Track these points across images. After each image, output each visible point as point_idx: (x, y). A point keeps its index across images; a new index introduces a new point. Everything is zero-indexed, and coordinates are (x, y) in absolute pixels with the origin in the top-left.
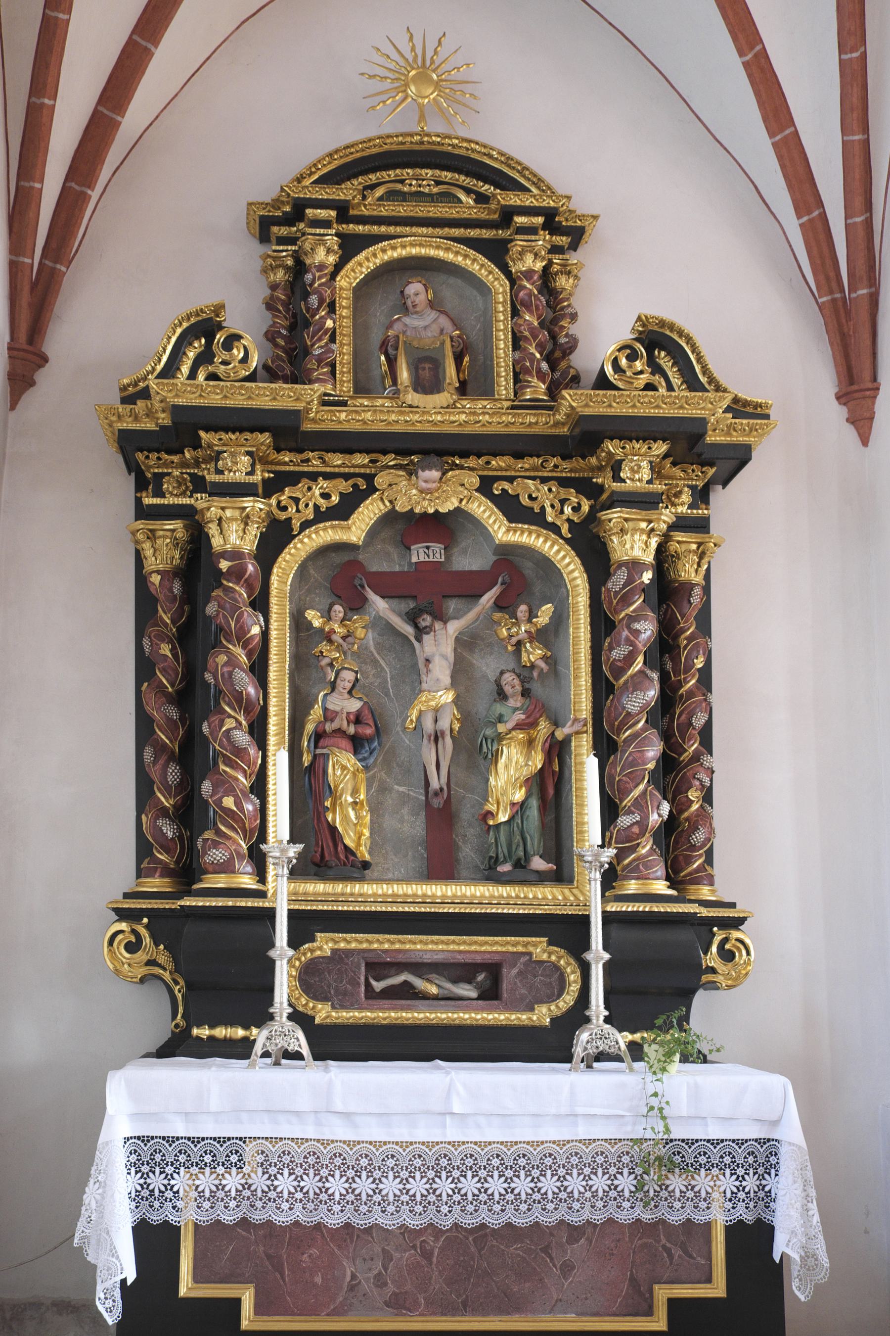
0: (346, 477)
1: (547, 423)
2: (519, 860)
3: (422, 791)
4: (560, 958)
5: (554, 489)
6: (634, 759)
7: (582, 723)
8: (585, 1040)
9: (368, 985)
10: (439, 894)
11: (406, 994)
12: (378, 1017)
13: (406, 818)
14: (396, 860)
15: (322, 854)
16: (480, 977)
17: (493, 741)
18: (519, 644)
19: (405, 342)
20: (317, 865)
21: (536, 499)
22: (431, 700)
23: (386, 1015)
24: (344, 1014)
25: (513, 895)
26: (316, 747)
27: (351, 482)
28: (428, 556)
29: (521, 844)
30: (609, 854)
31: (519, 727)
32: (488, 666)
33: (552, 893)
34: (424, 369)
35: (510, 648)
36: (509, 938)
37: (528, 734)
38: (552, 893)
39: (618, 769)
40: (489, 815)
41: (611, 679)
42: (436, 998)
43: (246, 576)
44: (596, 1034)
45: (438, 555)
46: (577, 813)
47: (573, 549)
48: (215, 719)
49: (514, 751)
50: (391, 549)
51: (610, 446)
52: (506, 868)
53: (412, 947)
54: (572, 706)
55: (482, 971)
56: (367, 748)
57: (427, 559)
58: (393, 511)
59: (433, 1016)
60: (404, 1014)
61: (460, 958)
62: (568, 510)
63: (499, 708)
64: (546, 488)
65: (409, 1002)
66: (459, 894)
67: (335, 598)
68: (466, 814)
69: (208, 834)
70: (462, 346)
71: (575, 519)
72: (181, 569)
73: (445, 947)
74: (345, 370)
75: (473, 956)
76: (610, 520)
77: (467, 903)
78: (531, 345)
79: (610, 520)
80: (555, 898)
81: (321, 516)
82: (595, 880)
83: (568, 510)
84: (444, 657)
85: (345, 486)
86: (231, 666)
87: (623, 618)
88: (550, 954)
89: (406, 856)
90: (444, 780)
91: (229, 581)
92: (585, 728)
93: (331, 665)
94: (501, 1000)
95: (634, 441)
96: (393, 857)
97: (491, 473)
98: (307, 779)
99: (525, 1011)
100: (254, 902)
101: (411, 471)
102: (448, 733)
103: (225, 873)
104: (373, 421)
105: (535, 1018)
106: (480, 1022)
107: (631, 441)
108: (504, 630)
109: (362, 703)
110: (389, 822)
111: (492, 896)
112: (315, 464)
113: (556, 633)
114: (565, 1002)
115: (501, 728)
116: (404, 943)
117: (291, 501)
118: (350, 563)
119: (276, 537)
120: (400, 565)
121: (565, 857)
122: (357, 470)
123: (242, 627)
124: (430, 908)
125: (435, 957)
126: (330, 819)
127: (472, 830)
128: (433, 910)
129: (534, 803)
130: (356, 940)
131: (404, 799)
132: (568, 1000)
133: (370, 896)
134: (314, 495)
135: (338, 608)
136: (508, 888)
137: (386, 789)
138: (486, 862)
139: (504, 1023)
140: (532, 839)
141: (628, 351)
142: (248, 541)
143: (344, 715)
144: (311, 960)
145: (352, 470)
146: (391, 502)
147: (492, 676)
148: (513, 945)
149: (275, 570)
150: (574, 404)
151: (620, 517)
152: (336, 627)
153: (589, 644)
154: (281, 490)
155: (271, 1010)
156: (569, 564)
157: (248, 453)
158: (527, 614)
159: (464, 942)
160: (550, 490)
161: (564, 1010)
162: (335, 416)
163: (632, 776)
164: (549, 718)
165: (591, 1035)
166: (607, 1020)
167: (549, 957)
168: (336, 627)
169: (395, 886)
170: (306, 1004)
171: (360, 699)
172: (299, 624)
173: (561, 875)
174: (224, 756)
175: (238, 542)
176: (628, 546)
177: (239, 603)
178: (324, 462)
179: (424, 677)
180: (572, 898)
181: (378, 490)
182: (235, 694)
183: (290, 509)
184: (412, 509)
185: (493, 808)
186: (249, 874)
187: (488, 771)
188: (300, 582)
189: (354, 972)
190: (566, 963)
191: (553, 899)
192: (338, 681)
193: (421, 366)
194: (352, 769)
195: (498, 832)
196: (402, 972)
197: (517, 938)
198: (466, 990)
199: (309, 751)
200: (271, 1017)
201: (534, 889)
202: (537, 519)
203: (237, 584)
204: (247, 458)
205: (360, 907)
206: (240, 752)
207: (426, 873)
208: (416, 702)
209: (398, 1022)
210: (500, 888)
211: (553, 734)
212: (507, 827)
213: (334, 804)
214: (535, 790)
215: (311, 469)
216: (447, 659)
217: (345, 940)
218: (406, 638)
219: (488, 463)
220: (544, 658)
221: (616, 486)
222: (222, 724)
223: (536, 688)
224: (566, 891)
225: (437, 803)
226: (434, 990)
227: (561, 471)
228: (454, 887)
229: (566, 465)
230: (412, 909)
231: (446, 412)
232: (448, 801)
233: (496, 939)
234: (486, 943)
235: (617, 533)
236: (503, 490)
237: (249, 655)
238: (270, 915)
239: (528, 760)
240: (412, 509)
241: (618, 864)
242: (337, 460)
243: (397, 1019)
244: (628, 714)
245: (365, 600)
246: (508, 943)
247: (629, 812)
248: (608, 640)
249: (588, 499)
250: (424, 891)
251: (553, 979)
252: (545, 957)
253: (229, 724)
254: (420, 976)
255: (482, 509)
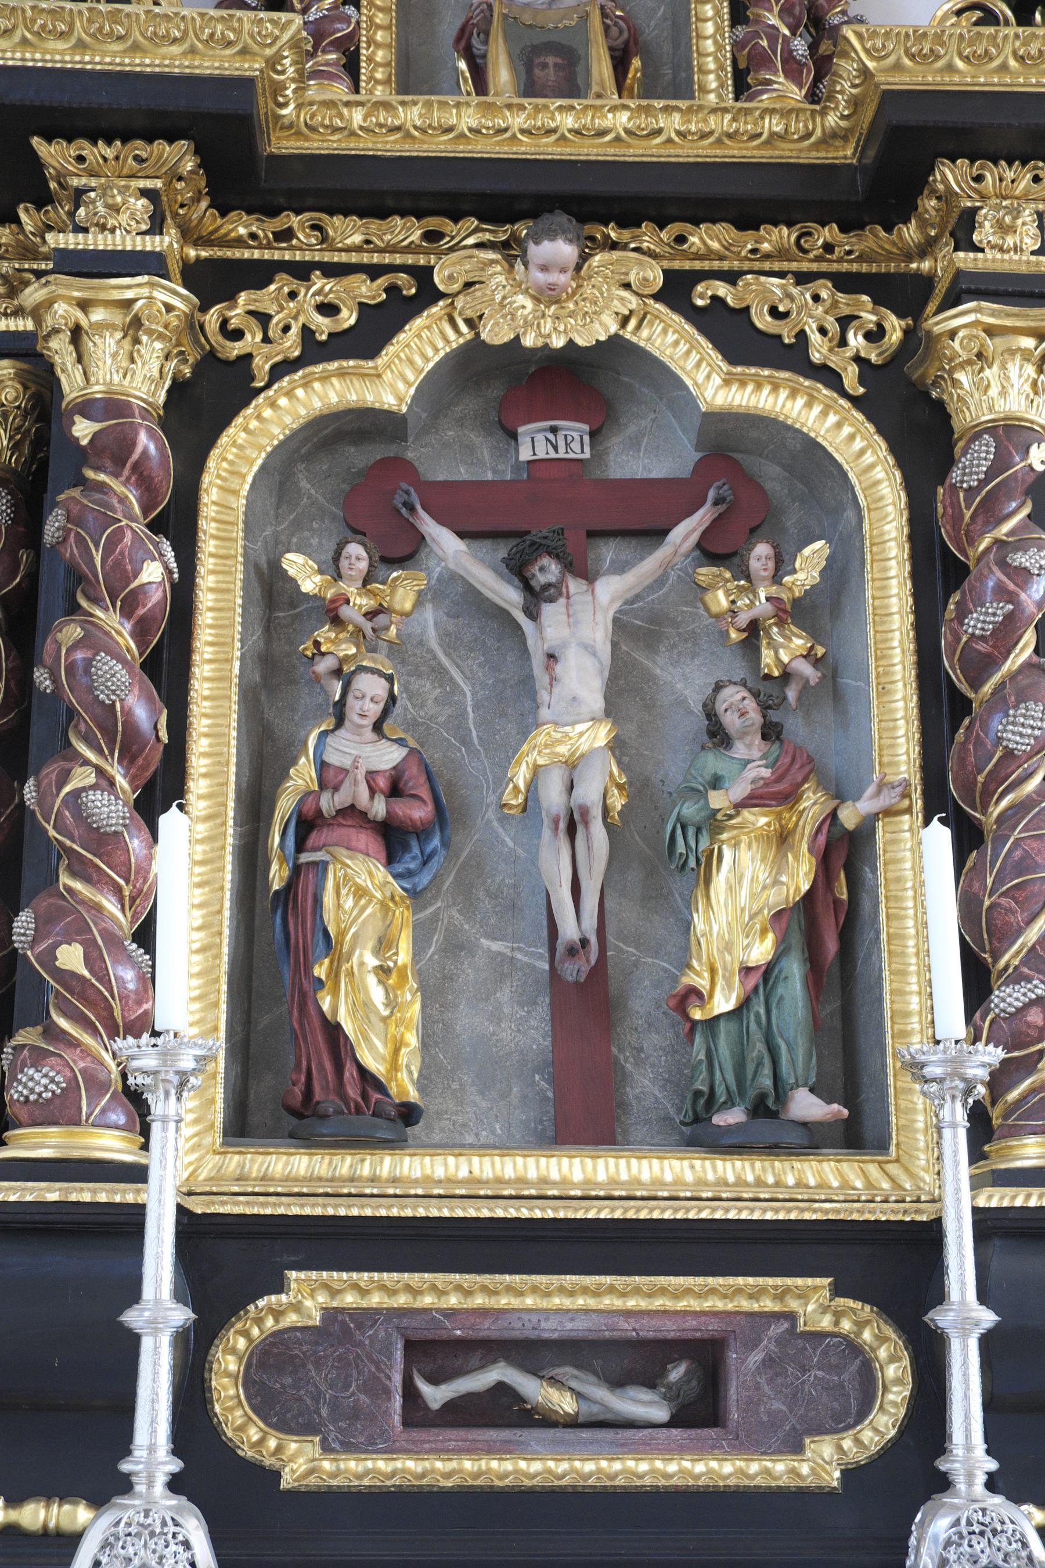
0: (374, 272)
1: (808, 135)
2: (762, 1097)
3: (544, 951)
4: (861, 1325)
5: (824, 294)
6: (1027, 855)
7: (899, 790)
8: (943, 1536)
9: (411, 1394)
10: (577, 1176)
11: (502, 1414)
12: (433, 1471)
13: (506, 1010)
14: (484, 1104)
15: (289, 1073)
16: (676, 1373)
17: (698, 831)
18: (754, 628)
19: (505, 17)
20: (299, 1115)
21: (786, 315)
22: (559, 742)
23: (453, 1465)
24: (352, 1464)
25: (750, 1178)
26: (300, 848)
27: (383, 281)
28: (556, 448)
29: (767, 1061)
30: (987, 1059)
31: (753, 800)
32: (684, 680)
33: (841, 1174)
34: (545, 66)
35: (734, 635)
36: (741, 1280)
37: (779, 817)
38: (841, 1174)
39: (989, 881)
40: (693, 998)
41: (963, 687)
42: (573, 1423)
43: (135, 456)
44: (969, 1523)
45: (576, 446)
46: (892, 992)
47: (870, 418)
48: (51, 771)
49: (745, 855)
50: (476, 438)
51: (950, 175)
52: (733, 1117)
53: (515, 1302)
54: (876, 754)
55: (680, 1359)
56: (416, 851)
57: (552, 455)
58: (476, 348)
59: (564, 1466)
60: (494, 1464)
61: (627, 1328)
62: (856, 341)
63: (712, 762)
64: (808, 296)
65: (506, 1434)
66: (624, 1177)
67: (350, 535)
68: (643, 1000)
69: (26, 1036)
70: (626, 35)
71: (873, 358)
72: (14, 471)
73: (591, 1303)
74: (379, 76)
75: (655, 1323)
76: (952, 334)
77: (643, 1198)
78: (771, 10)
79: (952, 334)
80: (845, 1185)
81: (315, 350)
82: (954, 1125)
83: (856, 341)
84: (590, 649)
85: (369, 290)
86: (88, 647)
87: (988, 550)
88: (838, 1316)
89: (505, 1095)
90: (590, 921)
91: (98, 469)
92: (906, 803)
93: (338, 673)
94: (724, 1426)
95: (1003, 163)
96: (478, 1099)
97: (687, 265)
98: (278, 920)
99: (781, 1452)
100: (115, 1192)
101: (511, 251)
102: (597, 813)
103: (55, 1123)
104: (423, 131)
105: (805, 1469)
106: (675, 1481)
107: (996, 163)
108: (721, 594)
109: (403, 752)
110: (468, 1021)
111: (702, 1183)
112: (304, 246)
113: (836, 609)
114: (876, 1430)
115: (717, 800)
116: (495, 1293)
117: (253, 322)
118: (386, 463)
119: (207, 397)
120: (495, 471)
121: (867, 1094)
122: (398, 259)
123: (118, 564)
124: (555, 1209)
125: (569, 1326)
126: (326, 1005)
127: (655, 1038)
128: (561, 1215)
129: (795, 969)
130: (383, 1288)
131: (503, 968)
132: (882, 1426)
133: (416, 1182)
134: (294, 310)
135: (355, 549)
136: (738, 1164)
137: (461, 947)
138: (688, 1104)
139: (732, 1482)
140: (790, 1049)
141: (978, 14)
142: (139, 378)
143: (361, 775)
144: (275, 1334)
145: (387, 259)
146: (469, 322)
147: (695, 702)
148: (751, 1297)
149: (211, 463)
150: (871, 65)
151: (976, 323)
152: (351, 590)
153: (911, 618)
154: (230, 297)
155: (125, 1467)
156: (862, 452)
157: (144, 193)
158: (771, 564)
159: (637, 1291)
160: (816, 298)
161: (874, 1450)
162: (341, 116)
163: (1021, 895)
164: (823, 784)
165: (957, 1523)
166: (992, 1484)
167: (837, 1323)
168: (351, 590)
169: (476, 1160)
170: (261, 1441)
171: (401, 742)
172: (270, 589)
173: (860, 1132)
174: (70, 851)
175: (116, 379)
176: (994, 391)
177: (115, 511)
178: (324, 239)
179: (544, 696)
180: (886, 1185)
181: (443, 296)
182: (98, 710)
183: (248, 337)
184: (517, 338)
185: (702, 982)
186: (117, 1127)
187: (689, 905)
188: (278, 507)
189: (377, 1364)
190: (877, 1337)
191: (841, 1187)
192: (350, 699)
193: (537, 61)
194: (378, 895)
195: (714, 1036)
196: (494, 1362)
197: (761, 1280)
198: (644, 1405)
199: (283, 859)
200: (125, 1485)
201: (797, 1165)
202: (790, 357)
203: (116, 475)
204: (144, 201)
205: (389, 1207)
206: (106, 842)
207: (550, 1133)
208: (525, 747)
209: (478, 1482)
210: (719, 1163)
211: (833, 815)
212: (733, 1026)
213: (335, 973)
214: (797, 940)
215: (298, 256)
216: (594, 654)
217: (355, 1286)
218: (503, 616)
219: (681, 239)
220: (808, 655)
221: (964, 259)
222: (64, 777)
223: (795, 726)
224: (873, 1169)
225: (573, 971)
226: (566, 1404)
227: (840, 260)
228: (611, 1161)
229: (845, 242)
230: (512, 1213)
231: (586, 108)
232: (599, 970)
233: (711, 1281)
234: (688, 1291)
235: (970, 362)
236: (715, 298)
237: (140, 633)
238: (130, 1223)
239: (779, 873)
240: (517, 338)
241: (993, 1103)
242: (349, 232)
243: (477, 1475)
244: (1009, 754)
245: (421, 539)
246: (739, 1291)
247: (1017, 978)
248: (956, 597)
249: (900, 316)
250: (543, 1172)
251: (846, 1376)
252: (826, 1323)
253: (82, 778)
254: (534, 1371)
255: (673, 343)
